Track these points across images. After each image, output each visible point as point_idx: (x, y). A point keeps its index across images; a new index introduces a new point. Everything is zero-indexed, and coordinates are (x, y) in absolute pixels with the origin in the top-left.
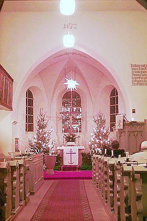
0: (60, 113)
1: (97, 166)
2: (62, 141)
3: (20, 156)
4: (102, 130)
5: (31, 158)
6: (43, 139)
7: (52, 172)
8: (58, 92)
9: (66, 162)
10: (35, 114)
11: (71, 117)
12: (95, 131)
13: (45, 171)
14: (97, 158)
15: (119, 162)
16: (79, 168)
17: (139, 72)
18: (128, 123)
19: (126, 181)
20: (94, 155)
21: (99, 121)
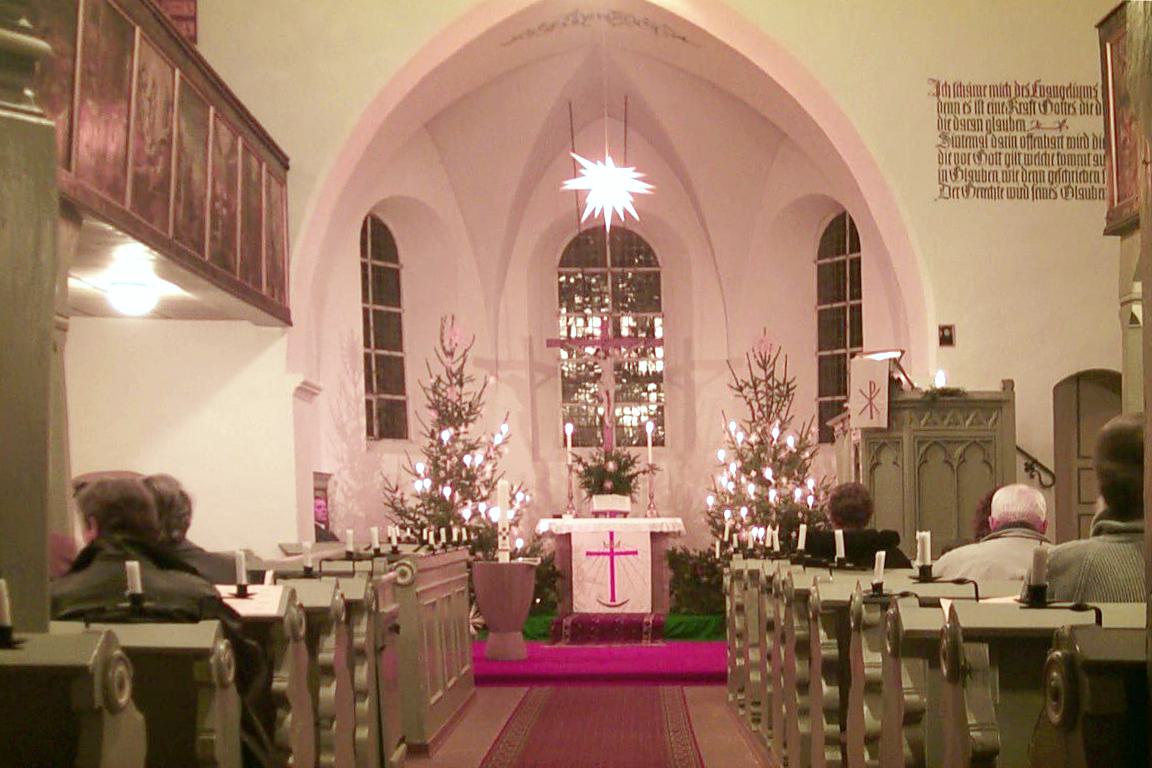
0: (552, 343)
1: (752, 613)
2: (565, 490)
3: (349, 556)
4: (775, 432)
5: (403, 574)
6: (466, 483)
7: (514, 646)
8: (528, 240)
9: (589, 597)
10: (357, 402)
11: (605, 368)
12: (740, 437)
13: (478, 646)
14: (754, 574)
15: (878, 587)
16: (658, 630)
17: (976, 125)
18: (919, 397)
19: (912, 684)
20: (738, 563)
21: (761, 387)
